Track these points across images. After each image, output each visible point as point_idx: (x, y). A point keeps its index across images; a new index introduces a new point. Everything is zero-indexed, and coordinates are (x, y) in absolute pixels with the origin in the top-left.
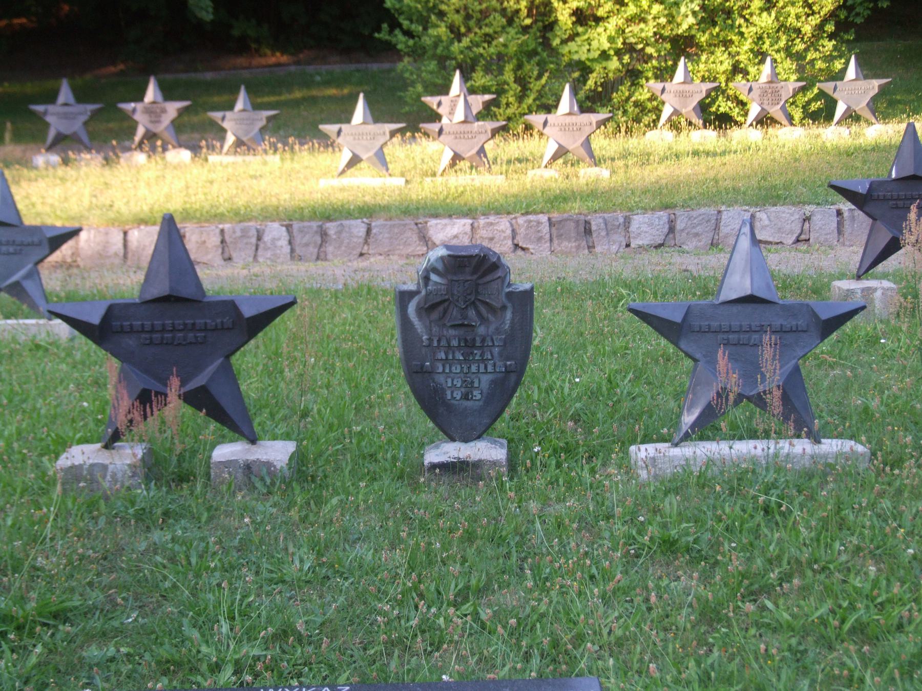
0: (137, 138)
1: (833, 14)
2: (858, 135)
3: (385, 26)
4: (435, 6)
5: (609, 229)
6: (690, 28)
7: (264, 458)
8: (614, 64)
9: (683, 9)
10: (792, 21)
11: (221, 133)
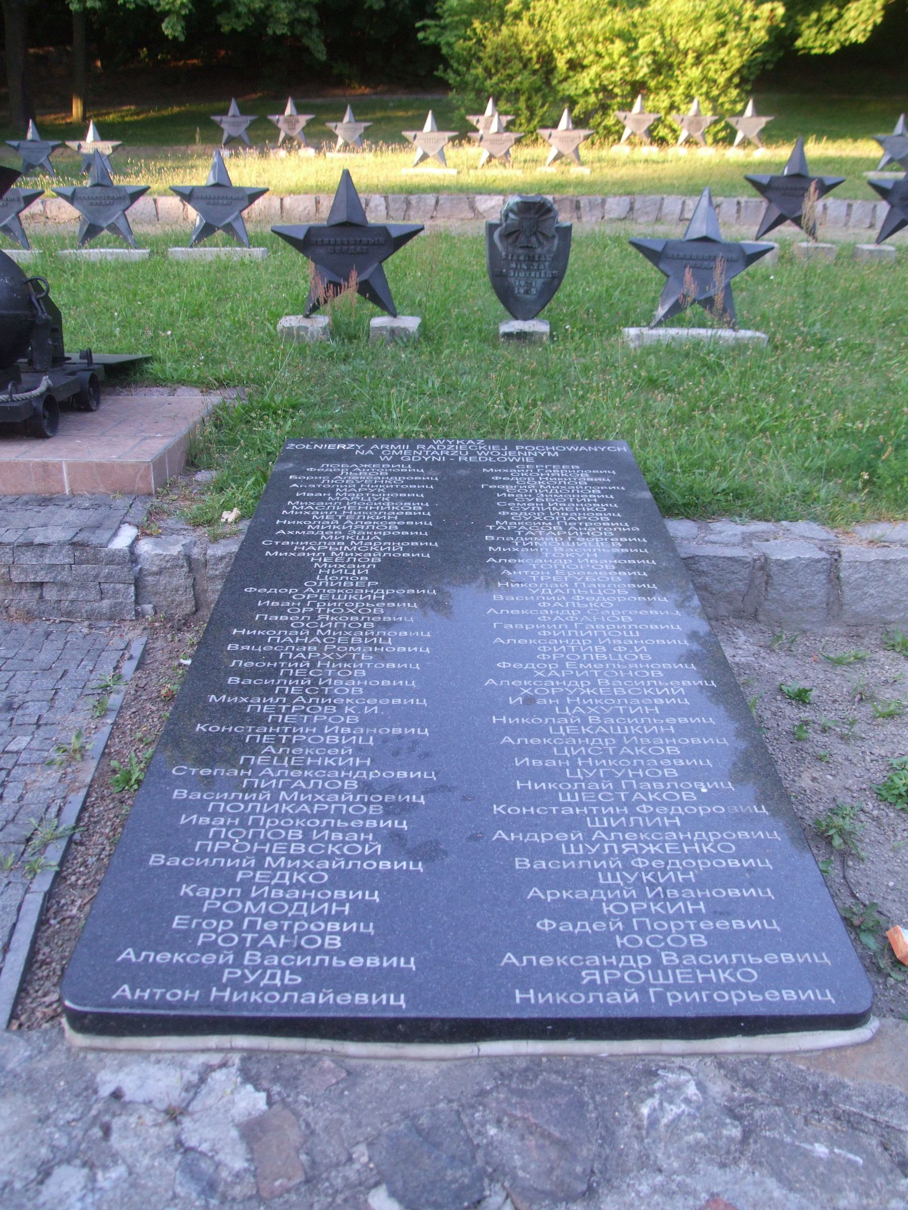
0: (281, 140)
1: (739, 71)
2: (748, 156)
3: (441, 67)
4: (475, 54)
5: (592, 206)
6: (645, 76)
7: (402, 326)
8: (592, 99)
9: (641, 62)
10: (711, 74)
11: (333, 137)
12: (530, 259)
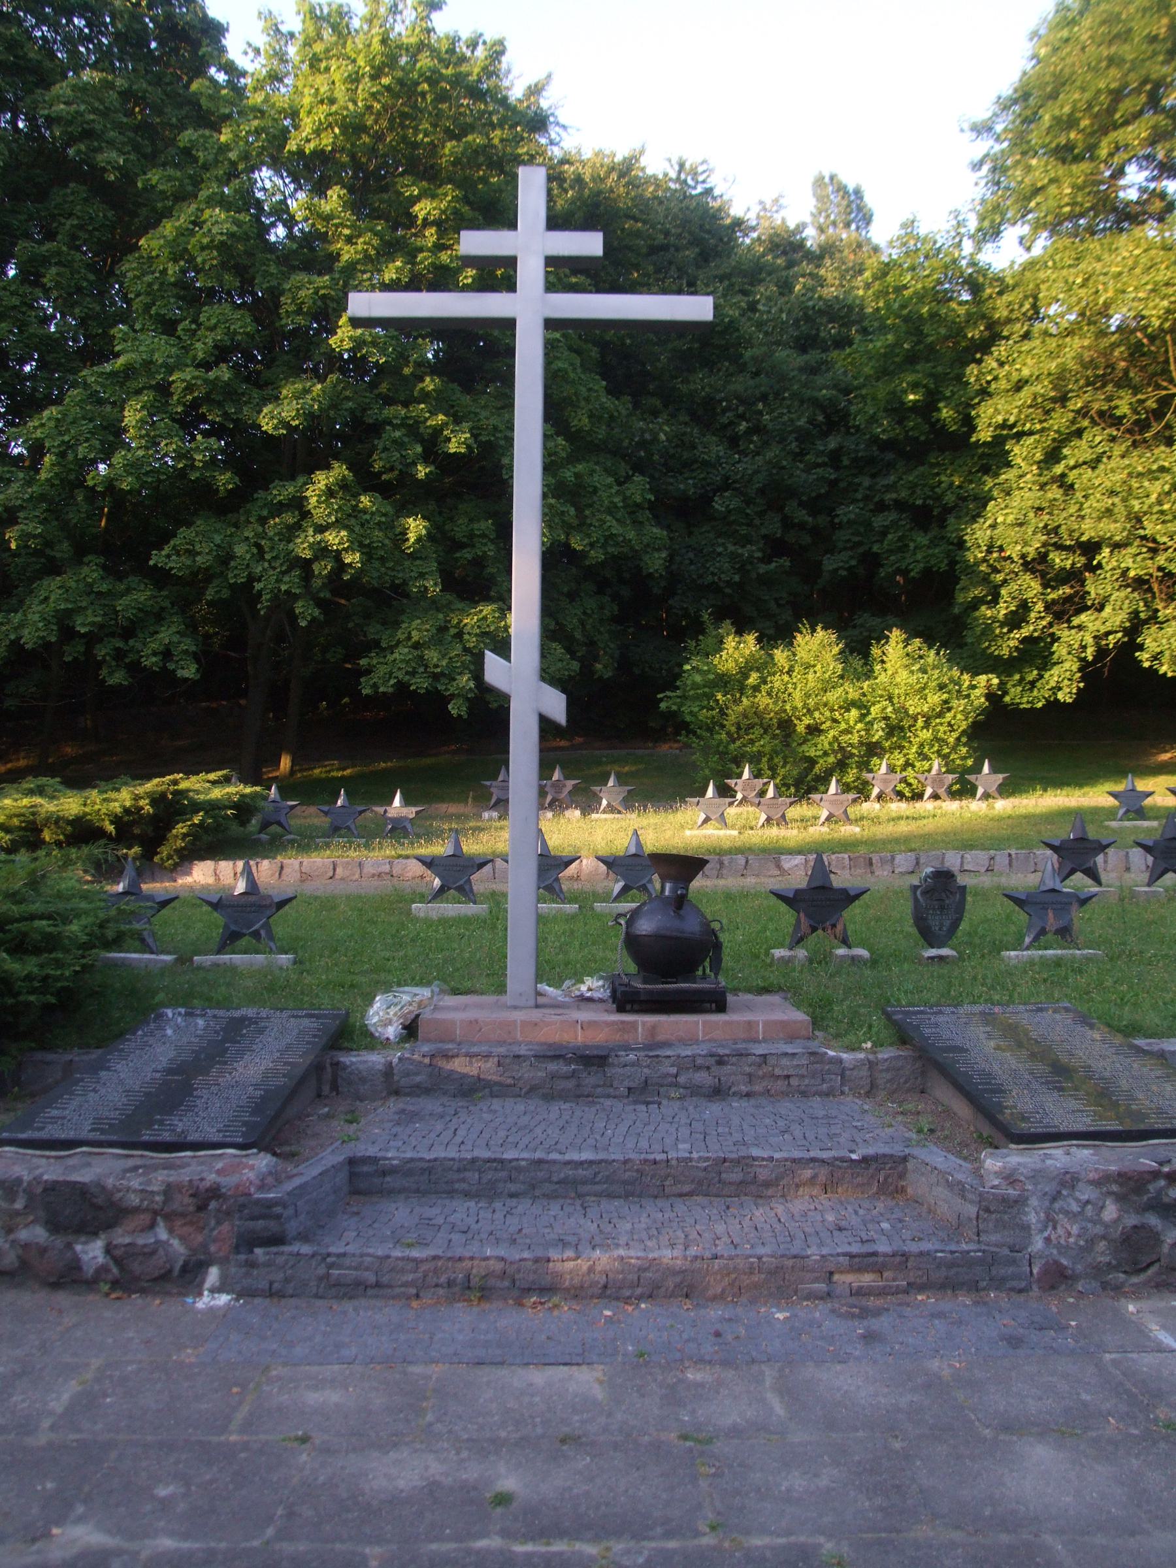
8: (831, 759)
12: (942, 908)
